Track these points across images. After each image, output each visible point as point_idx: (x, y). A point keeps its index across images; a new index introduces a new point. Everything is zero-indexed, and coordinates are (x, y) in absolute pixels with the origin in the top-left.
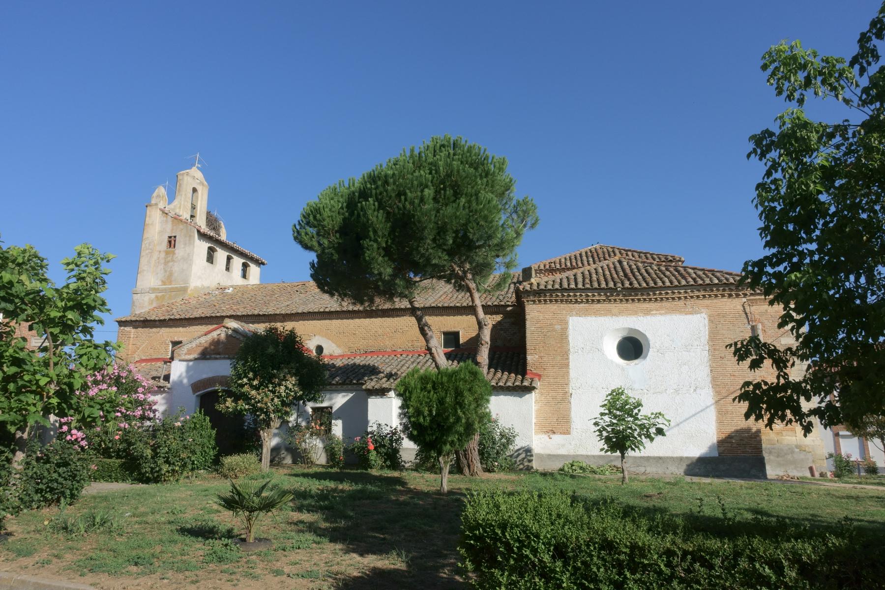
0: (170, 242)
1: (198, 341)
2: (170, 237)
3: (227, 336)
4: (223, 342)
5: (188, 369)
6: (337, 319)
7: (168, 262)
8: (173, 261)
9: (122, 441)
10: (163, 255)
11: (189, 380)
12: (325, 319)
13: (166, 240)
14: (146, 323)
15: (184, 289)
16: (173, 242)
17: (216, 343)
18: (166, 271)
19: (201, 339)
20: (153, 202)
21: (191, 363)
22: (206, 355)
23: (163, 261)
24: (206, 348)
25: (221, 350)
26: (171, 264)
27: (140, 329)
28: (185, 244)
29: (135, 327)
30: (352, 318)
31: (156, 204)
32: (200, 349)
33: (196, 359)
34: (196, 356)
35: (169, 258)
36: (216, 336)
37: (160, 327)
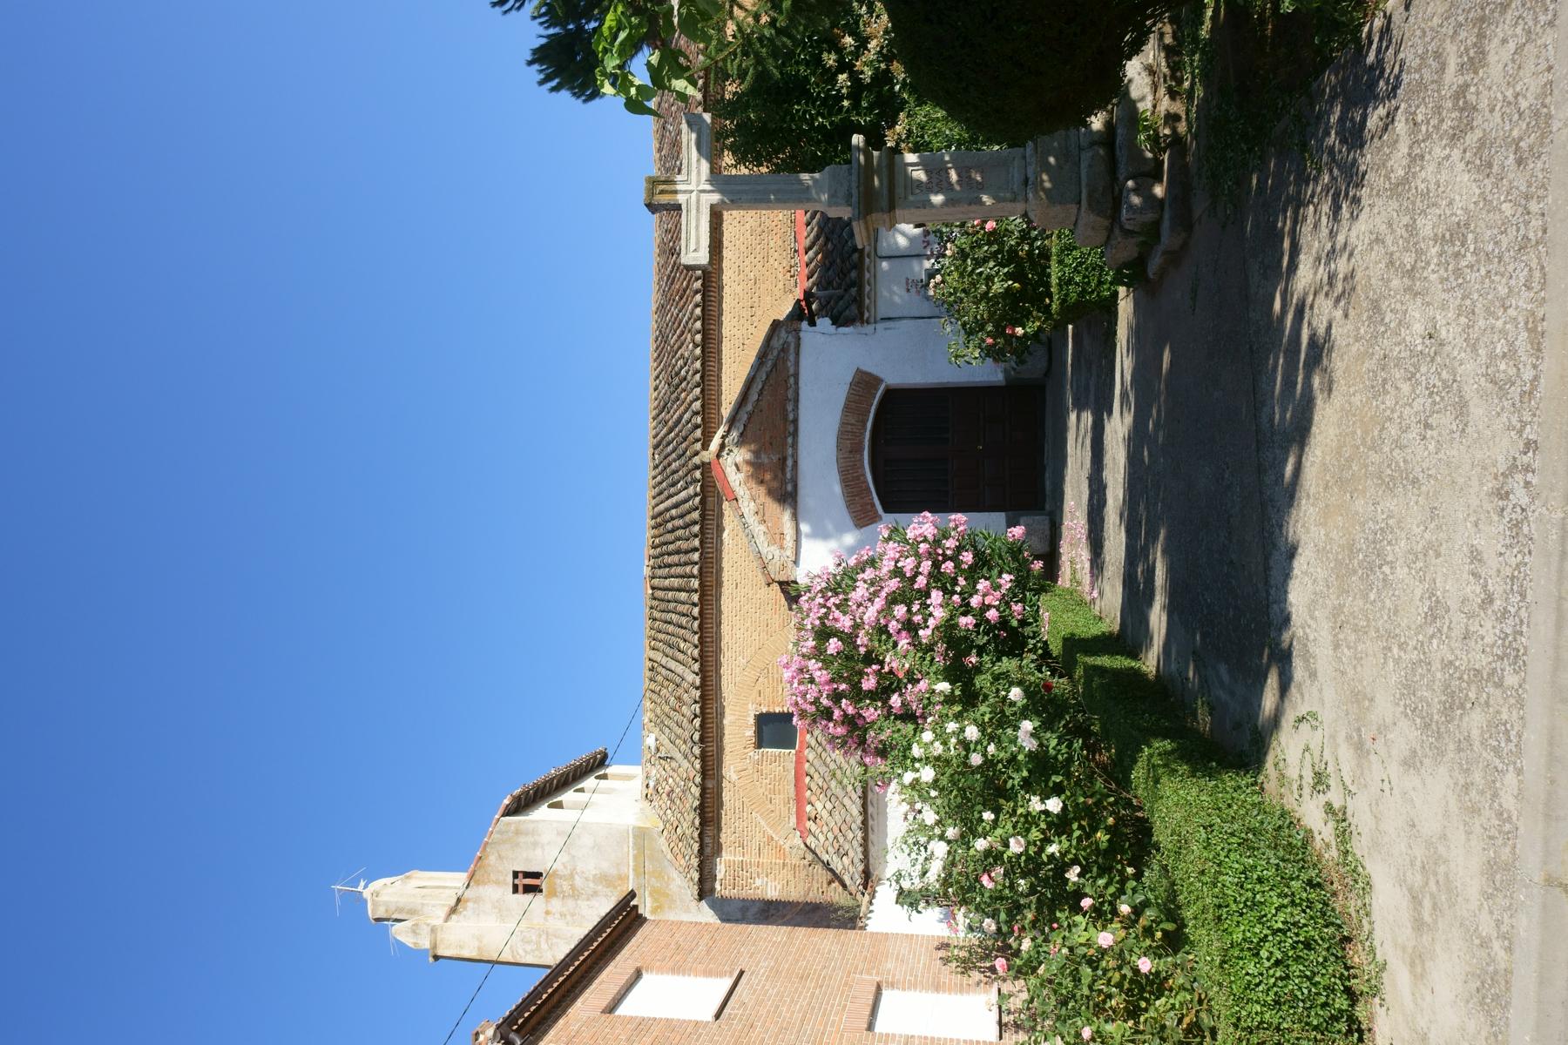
0: (529, 889)
1: (752, 520)
2: (515, 889)
3: (741, 442)
4: (756, 453)
5: (820, 534)
6: (720, 324)
7: (573, 887)
8: (572, 876)
9: (994, 915)
10: (556, 904)
11: (848, 531)
12: (720, 352)
13: (524, 899)
14: (709, 813)
15: (641, 835)
16: (528, 881)
17: (757, 470)
18: (595, 894)
19: (745, 511)
20: (425, 944)
21: (805, 528)
22: (786, 493)
23: (570, 903)
24: (770, 493)
25: (775, 458)
26: (578, 881)
27: (723, 837)
28: (535, 844)
29: (718, 850)
30: (721, 288)
31: (433, 930)
32: (772, 507)
33: (795, 517)
34: (787, 516)
35: (566, 887)
36: (741, 476)
37: (719, 779)
